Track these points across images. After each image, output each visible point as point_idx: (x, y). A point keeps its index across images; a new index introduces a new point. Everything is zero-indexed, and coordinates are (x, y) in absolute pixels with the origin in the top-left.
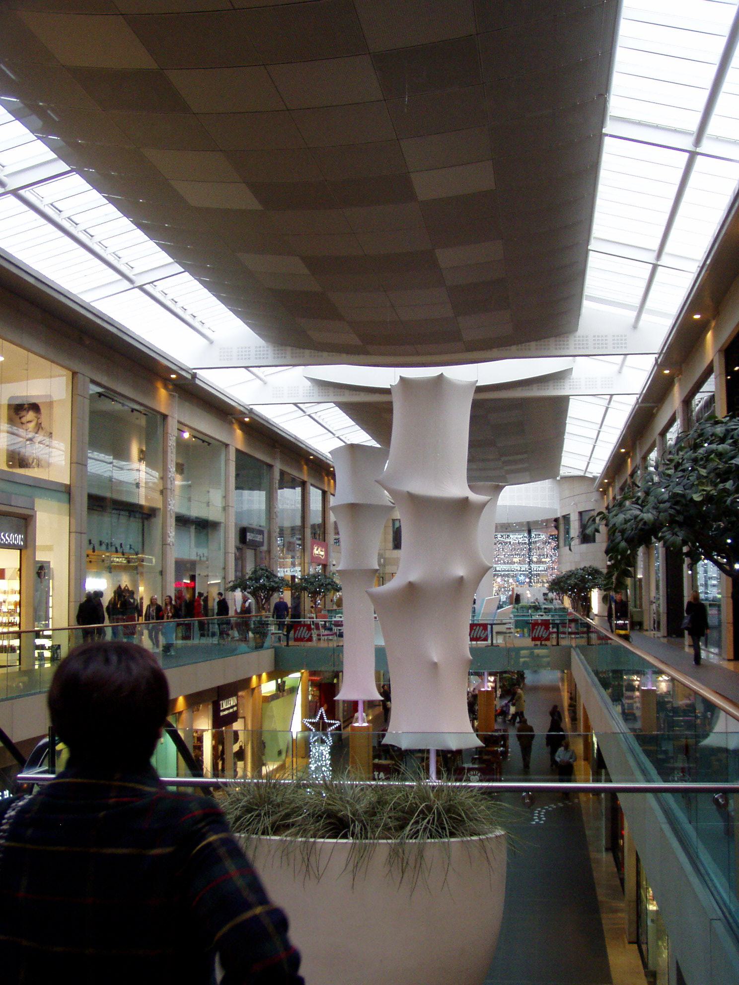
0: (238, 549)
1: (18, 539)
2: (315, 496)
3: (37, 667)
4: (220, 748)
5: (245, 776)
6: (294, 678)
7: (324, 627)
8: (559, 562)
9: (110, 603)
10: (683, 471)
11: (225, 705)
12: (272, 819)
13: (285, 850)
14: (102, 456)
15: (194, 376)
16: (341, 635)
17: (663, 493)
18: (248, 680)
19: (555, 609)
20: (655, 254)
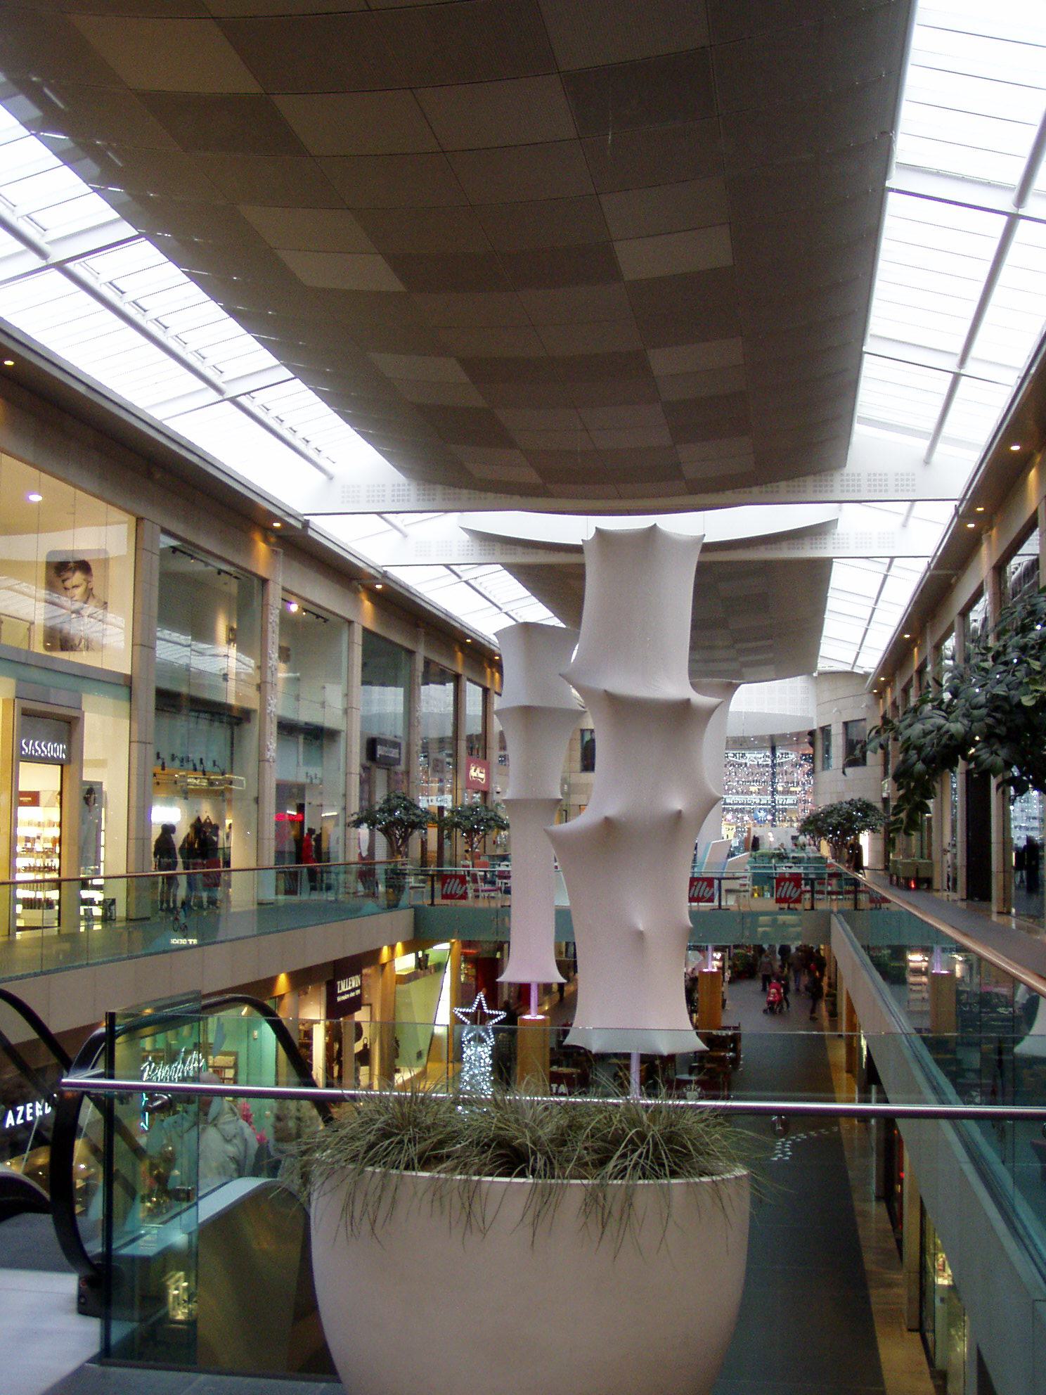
0: (364, 768)
1: (59, 750)
2: (473, 694)
3: (82, 929)
4: (337, 1046)
5: (370, 1087)
6: (440, 950)
7: (484, 879)
8: (815, 792)
9: (184, 841)
10: (1006, 663)
11: (343, 986)
12: (420, 1147)
13: (436, 1189)
14: (176, 636)
15: (306, 524)
16: (508, 891)
17: (977, 695)
20: (957, 359)
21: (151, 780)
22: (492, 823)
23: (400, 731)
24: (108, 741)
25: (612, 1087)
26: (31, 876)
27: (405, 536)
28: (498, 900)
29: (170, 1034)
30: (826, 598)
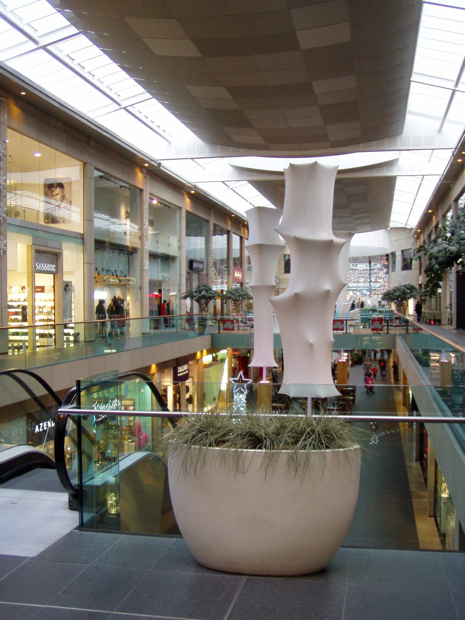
0: (188, 273)
1: (52, 268)
2: (236, 239)
3: (65, 346)
4: (178, 396)
5: (193, 412)
6: (223, 353)
7: (242, 321)
8: (389, 282)
11: (180, 369)
12: (215, 437)
13: (223, 455)
14: (103, 216)
15: (159, 164)
16: (252, 327)
18: (195, 355)
19: (386, 311)
20: (454, 83)
21: (93, 280)
22: (245, 296)
23: (203, 257)
24: (74, 262)
25: (299, 410)
26: (42, 323)
27: (204, 169)
28: (248, 331)
29: (105, 391)
30: (393, 194)
